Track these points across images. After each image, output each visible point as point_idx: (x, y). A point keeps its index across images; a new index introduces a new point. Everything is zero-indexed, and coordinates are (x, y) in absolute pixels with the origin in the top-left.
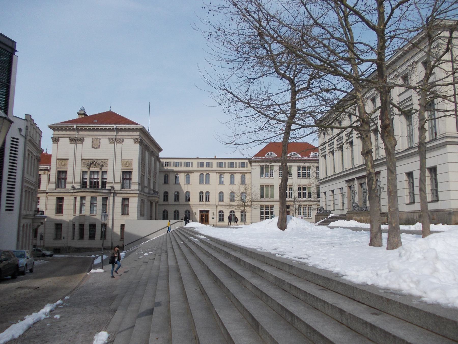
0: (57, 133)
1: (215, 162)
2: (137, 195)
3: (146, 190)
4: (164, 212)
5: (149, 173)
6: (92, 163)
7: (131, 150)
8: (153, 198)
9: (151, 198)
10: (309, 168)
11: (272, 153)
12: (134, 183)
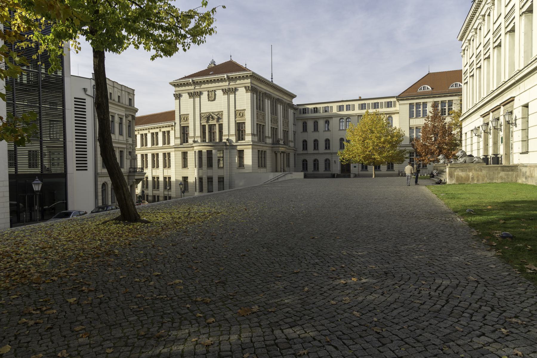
0: (178, 89)
1: (357, 104)
2: (251, 146)
3: (269, 141)
4: (303, 161)
6: (209, 117)
7: (244, 100)
8: (277, 149)
9: (274, 149)
10: (425, 104)
11: (426, 86)
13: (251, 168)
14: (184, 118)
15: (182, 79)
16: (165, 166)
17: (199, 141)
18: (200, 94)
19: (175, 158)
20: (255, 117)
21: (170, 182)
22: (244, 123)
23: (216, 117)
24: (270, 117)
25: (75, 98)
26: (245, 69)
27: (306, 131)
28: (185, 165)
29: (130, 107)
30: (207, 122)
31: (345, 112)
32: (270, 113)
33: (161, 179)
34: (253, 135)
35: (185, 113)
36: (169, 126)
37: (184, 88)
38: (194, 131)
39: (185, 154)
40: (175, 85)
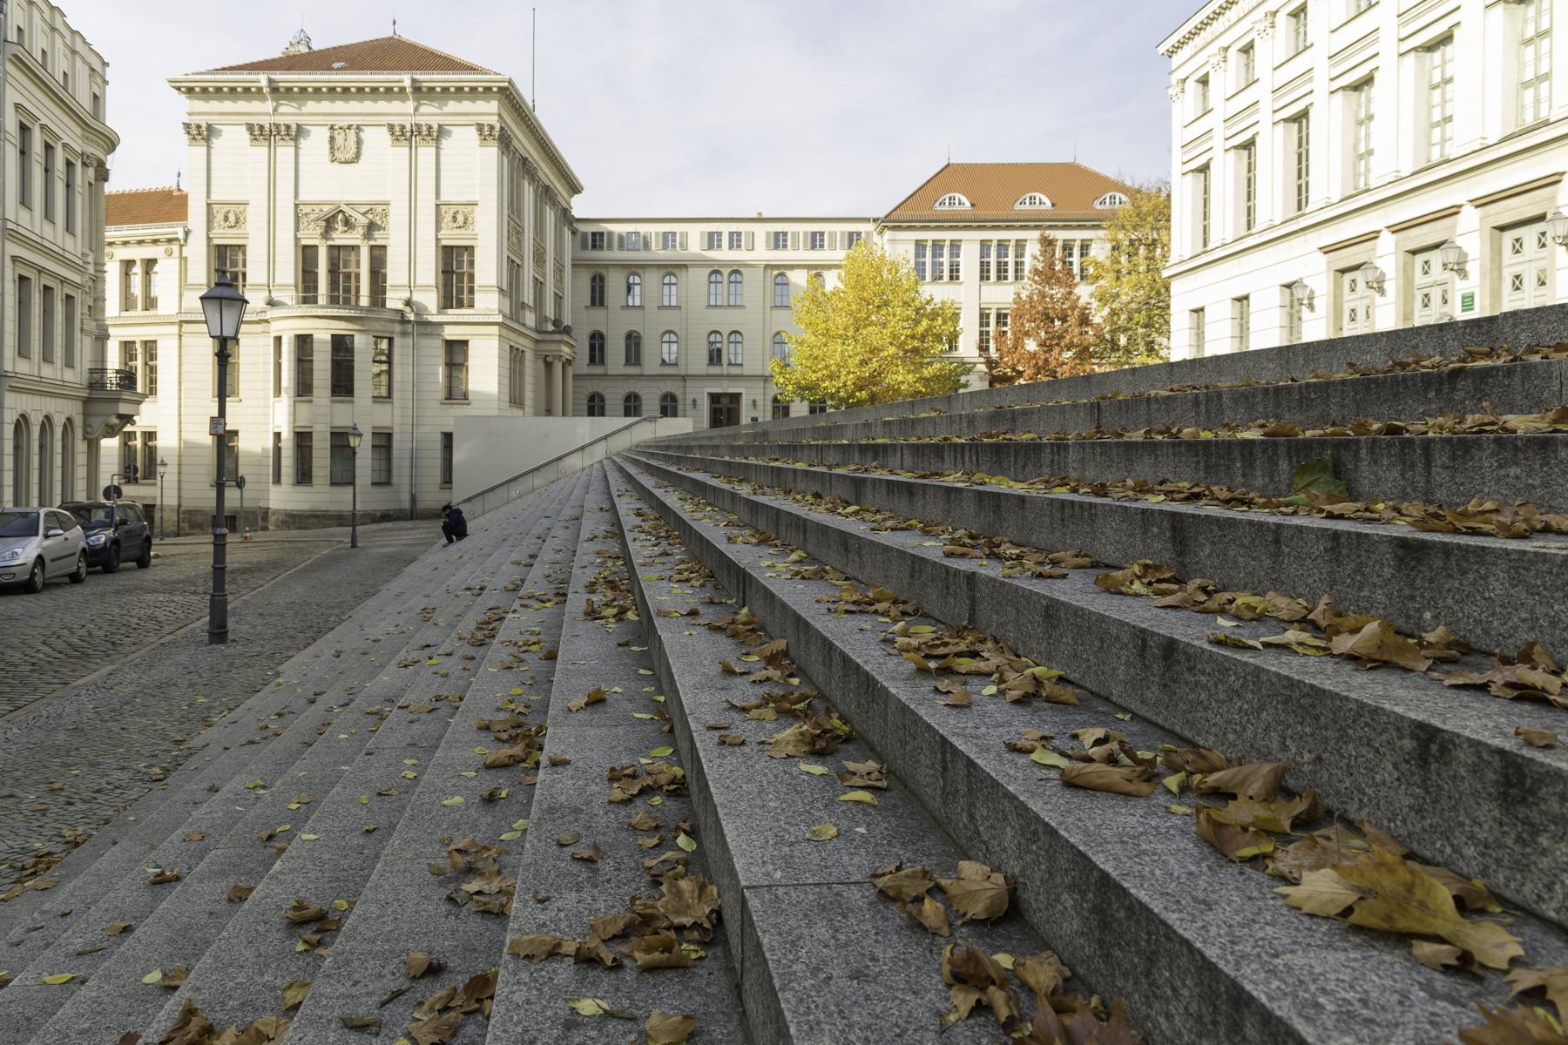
0: (200, 105)
1: (761, 230)
2: (496, 328)
3: (530, 319)
5: (539, 259)
7: (473, 169)
8: (554, 347)
11: (957, 195)
13: (495, 404)
18: (296, 134)
23: (364, 221)
26: (471, 69)
27: (602, 304)
30: (326, 234)
31: (724, 254)
36: (155, 242)
37: (227, 106)
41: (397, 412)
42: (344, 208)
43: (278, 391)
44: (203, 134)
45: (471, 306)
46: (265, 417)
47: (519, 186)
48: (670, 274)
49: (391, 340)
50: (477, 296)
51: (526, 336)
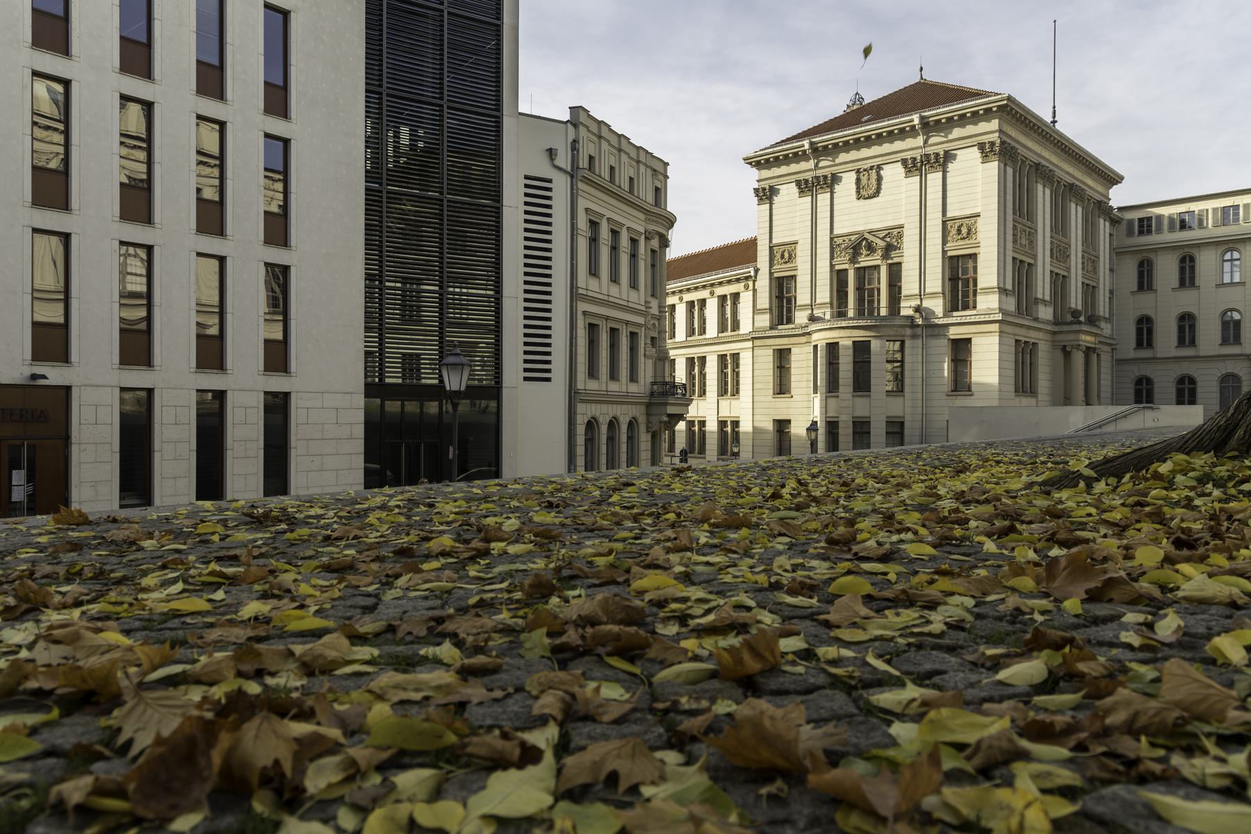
0: (766, 173)
2: (996, 327)
3: (1045, 313)
6: (859, 245)
7: (975, 184)
8: (1072, 337)
9: (1060, 337)
12: (987, 290)
13: (996, 395)
14: (783, 253)
15: (778, 144)
16: (722, 392)
17: (828, 317)
18: (830, 182)
19: (755, 367)
20: (1010, 238)
21: (736, 435)
22: (973, 257)
23: (882, 244)
24: (1048, 240)
25: (527, 177)
26: (997, 94)
27: (1192, 283)
28: (782, 387)
29: (656, 210)
30: (853, 260)
32: (1048, 229)
33: (712, 426)
34: (1002, 291)
35: (786, 240)
36: (738, 280)
38: (813, 288)
39: (782, 358)
40: (759, 162)
41: (908, 403)
42: (867, 236)
43: (815, 391)
44: (766, 195)
45: (975, 307)
46: (806, 408)
47: (1031, 193)
48: (1232, 250)
49: (903, 343)
50: (979, 298)
51: (1039, 329)
